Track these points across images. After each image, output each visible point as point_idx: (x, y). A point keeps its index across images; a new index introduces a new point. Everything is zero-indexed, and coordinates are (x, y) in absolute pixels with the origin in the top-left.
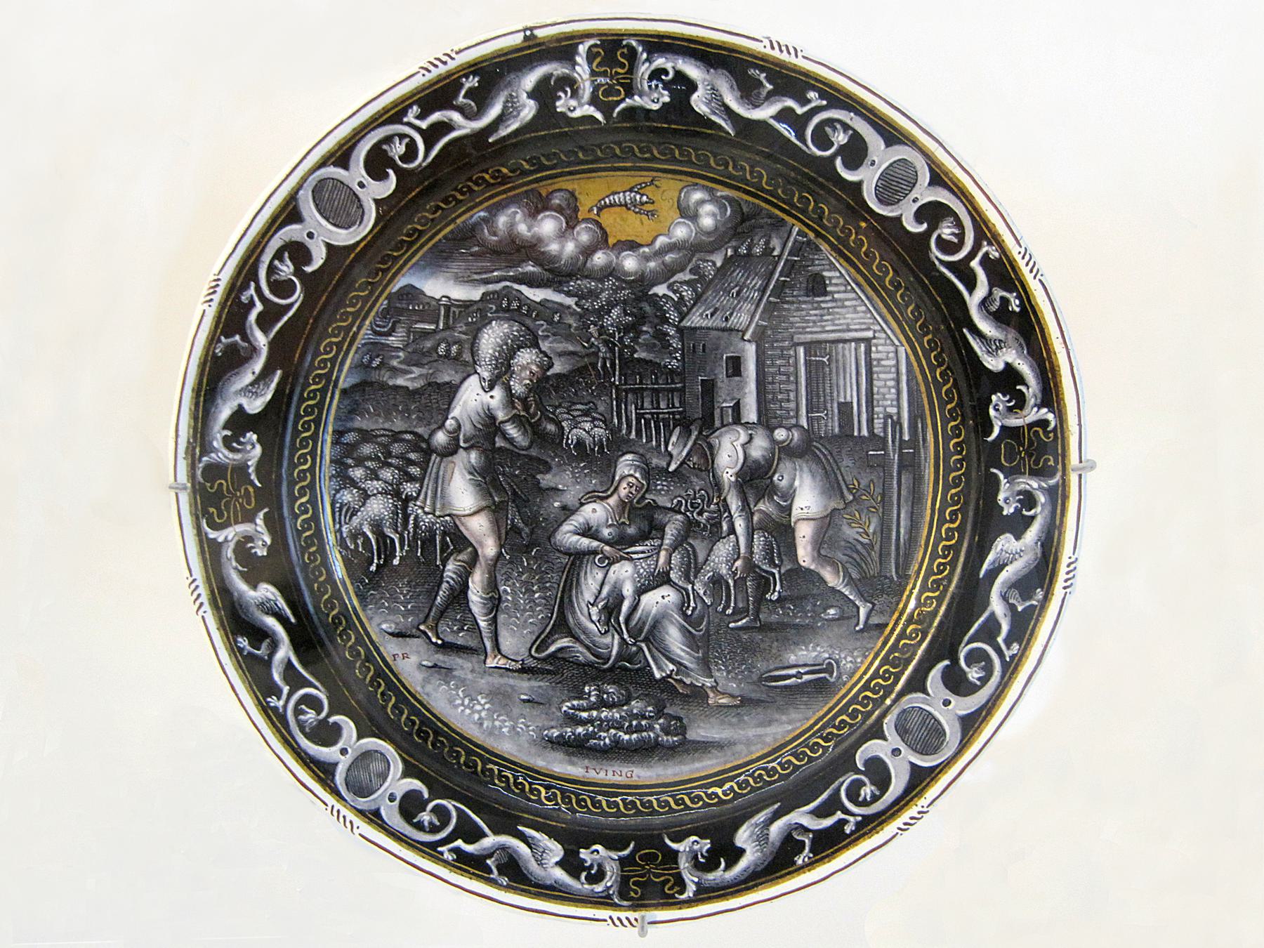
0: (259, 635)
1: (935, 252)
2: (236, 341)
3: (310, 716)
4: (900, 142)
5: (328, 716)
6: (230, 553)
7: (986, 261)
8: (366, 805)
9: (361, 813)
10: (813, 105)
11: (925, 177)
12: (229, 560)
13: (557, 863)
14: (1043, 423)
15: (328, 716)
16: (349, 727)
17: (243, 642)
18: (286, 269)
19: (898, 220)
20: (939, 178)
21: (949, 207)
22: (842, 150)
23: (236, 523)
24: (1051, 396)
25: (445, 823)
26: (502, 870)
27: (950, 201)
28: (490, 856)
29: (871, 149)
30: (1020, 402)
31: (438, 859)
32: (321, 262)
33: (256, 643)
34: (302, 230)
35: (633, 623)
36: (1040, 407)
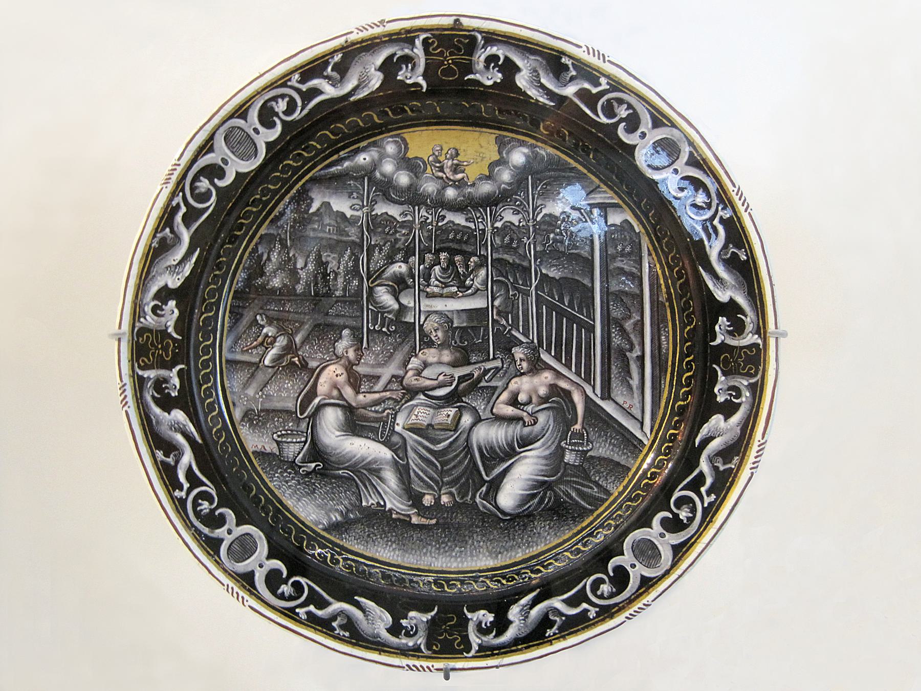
0: (545, 622)
1: (296, 116)
2: (337, 625)
3: (605, 588)
4: (675, 556)
5: (607, 574)
6: (407, 51)
7: (303, 81)
8: (667, 552)
9: (211, 137)
10: (705, 497)
11: (649, 573)
12: (402, 49)
13: (726, 420)
14: (425, 42)
15: (607, 574)
16: (274, 134)
17: (338, 58)
18: (286, 589)
19: (269, 145)
20: (647, 584)
21: (624, 590)
22: (676, 516)
23: (426, 60)
24: (486, 651)
25: (691, 501)
26: (163, 240)
27: (632, 587)
28: (172, 231)
29: (214, 162)
30: (407, 59)
31: (173, 194)
32: (279, 563)
33: (551, 624)
34: (259, 571)
35: (406, 348)
36: (480, 645)
